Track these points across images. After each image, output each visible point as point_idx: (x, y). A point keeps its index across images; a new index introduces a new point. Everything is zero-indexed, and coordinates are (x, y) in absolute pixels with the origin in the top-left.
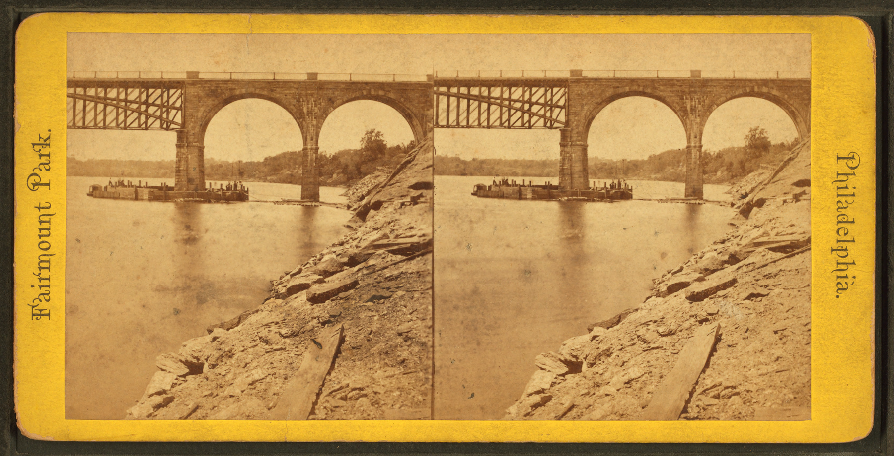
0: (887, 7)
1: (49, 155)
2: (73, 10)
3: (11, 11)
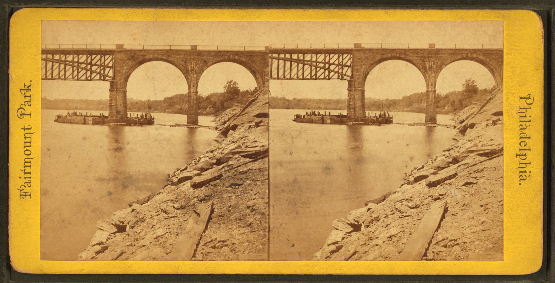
0: (551, 4)
1: (30, 96)
2: (45, 6)
3: (7, 7)
